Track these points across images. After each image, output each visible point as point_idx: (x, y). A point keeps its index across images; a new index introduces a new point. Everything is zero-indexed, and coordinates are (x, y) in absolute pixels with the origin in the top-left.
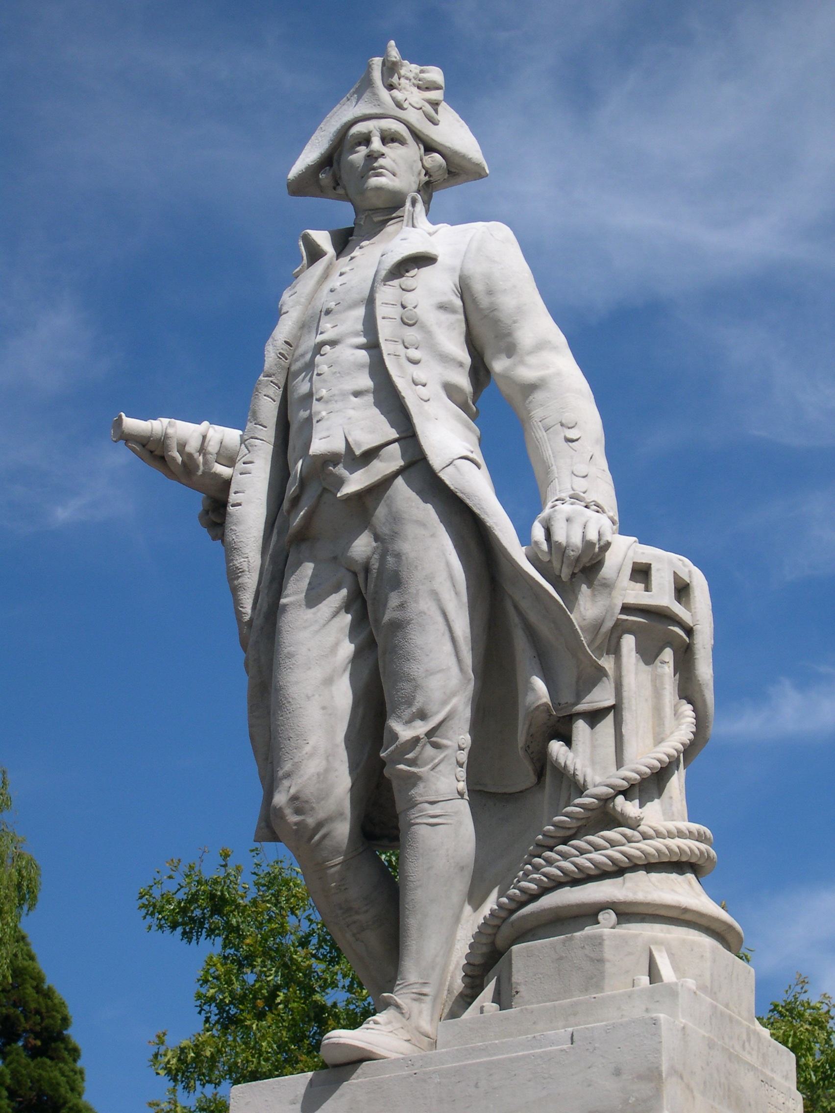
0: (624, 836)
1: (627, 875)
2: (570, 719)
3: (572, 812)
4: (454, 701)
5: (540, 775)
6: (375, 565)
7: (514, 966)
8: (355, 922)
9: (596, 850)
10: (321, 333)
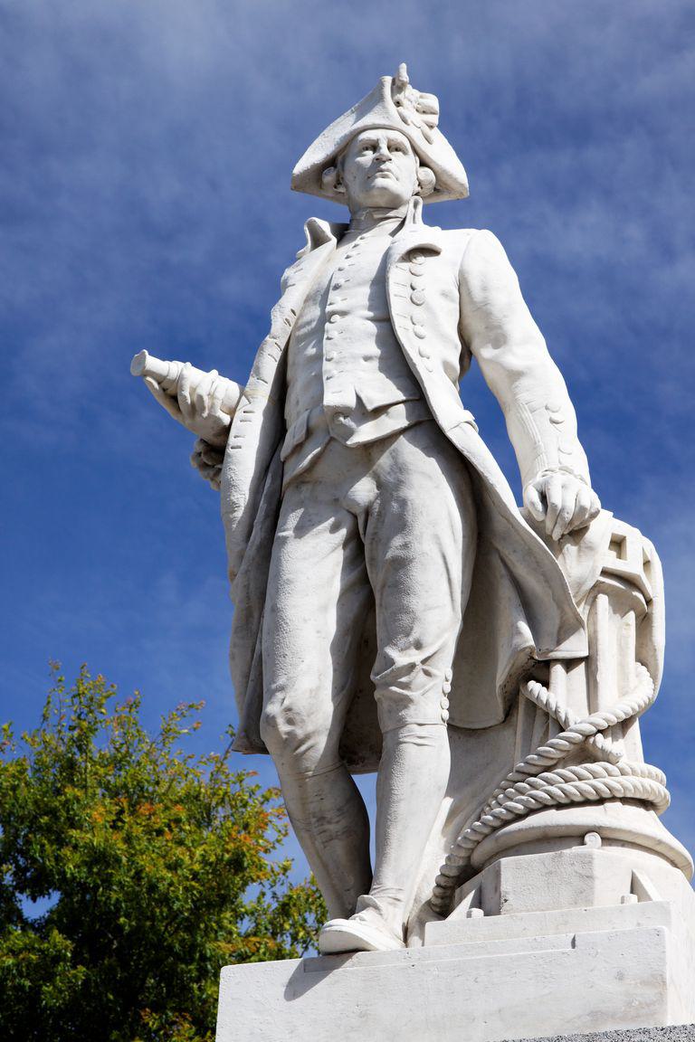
0: (606, 770)
1: (608, 805)
2: (547, 664)
3: (557, 744)
4: (446, 635)
5: (510, 710)
6: (376, 507)
7: (502, 876)
8: (324, 831)
9: (566, 782)
10: (331, 304)
